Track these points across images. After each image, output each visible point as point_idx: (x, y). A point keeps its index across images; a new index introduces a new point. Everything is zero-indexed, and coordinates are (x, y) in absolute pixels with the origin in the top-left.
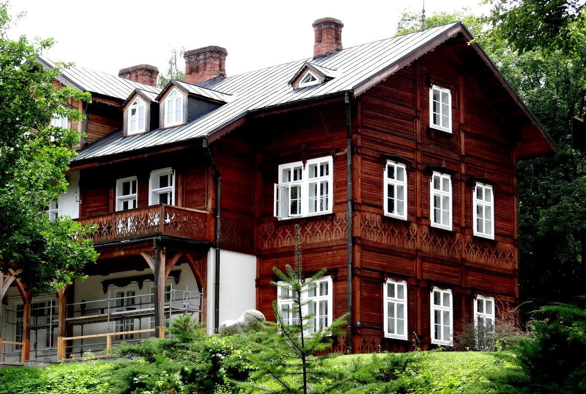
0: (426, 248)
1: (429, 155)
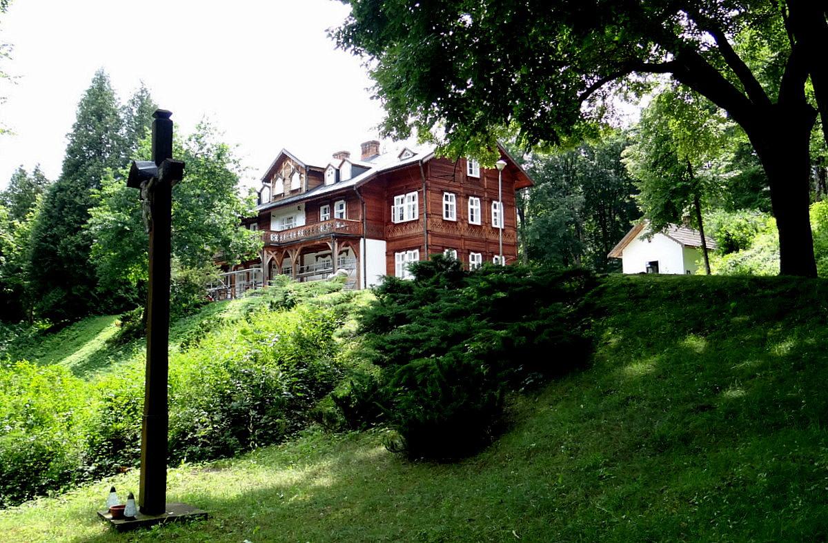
0: (467, 234)
1: (468, 188)
